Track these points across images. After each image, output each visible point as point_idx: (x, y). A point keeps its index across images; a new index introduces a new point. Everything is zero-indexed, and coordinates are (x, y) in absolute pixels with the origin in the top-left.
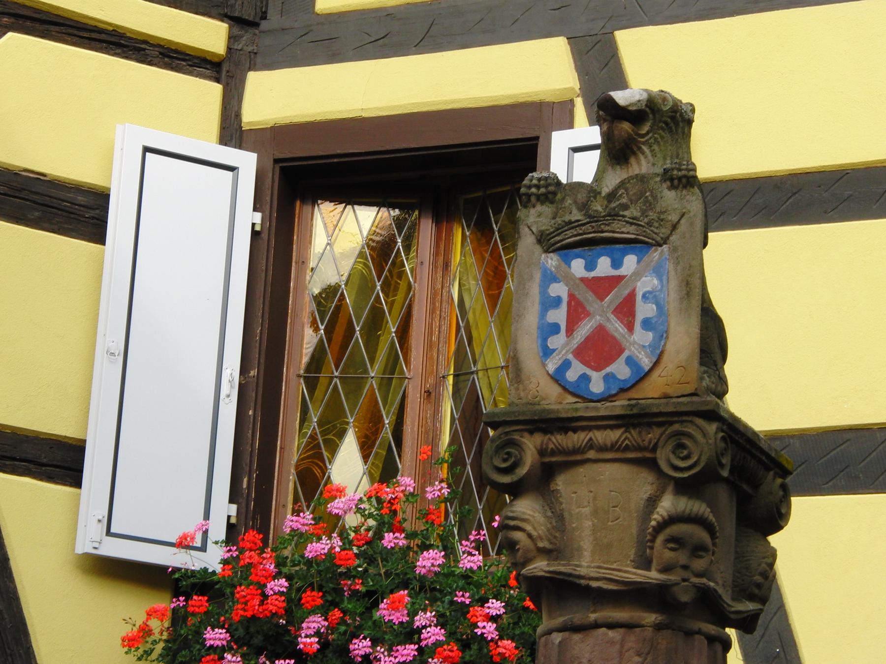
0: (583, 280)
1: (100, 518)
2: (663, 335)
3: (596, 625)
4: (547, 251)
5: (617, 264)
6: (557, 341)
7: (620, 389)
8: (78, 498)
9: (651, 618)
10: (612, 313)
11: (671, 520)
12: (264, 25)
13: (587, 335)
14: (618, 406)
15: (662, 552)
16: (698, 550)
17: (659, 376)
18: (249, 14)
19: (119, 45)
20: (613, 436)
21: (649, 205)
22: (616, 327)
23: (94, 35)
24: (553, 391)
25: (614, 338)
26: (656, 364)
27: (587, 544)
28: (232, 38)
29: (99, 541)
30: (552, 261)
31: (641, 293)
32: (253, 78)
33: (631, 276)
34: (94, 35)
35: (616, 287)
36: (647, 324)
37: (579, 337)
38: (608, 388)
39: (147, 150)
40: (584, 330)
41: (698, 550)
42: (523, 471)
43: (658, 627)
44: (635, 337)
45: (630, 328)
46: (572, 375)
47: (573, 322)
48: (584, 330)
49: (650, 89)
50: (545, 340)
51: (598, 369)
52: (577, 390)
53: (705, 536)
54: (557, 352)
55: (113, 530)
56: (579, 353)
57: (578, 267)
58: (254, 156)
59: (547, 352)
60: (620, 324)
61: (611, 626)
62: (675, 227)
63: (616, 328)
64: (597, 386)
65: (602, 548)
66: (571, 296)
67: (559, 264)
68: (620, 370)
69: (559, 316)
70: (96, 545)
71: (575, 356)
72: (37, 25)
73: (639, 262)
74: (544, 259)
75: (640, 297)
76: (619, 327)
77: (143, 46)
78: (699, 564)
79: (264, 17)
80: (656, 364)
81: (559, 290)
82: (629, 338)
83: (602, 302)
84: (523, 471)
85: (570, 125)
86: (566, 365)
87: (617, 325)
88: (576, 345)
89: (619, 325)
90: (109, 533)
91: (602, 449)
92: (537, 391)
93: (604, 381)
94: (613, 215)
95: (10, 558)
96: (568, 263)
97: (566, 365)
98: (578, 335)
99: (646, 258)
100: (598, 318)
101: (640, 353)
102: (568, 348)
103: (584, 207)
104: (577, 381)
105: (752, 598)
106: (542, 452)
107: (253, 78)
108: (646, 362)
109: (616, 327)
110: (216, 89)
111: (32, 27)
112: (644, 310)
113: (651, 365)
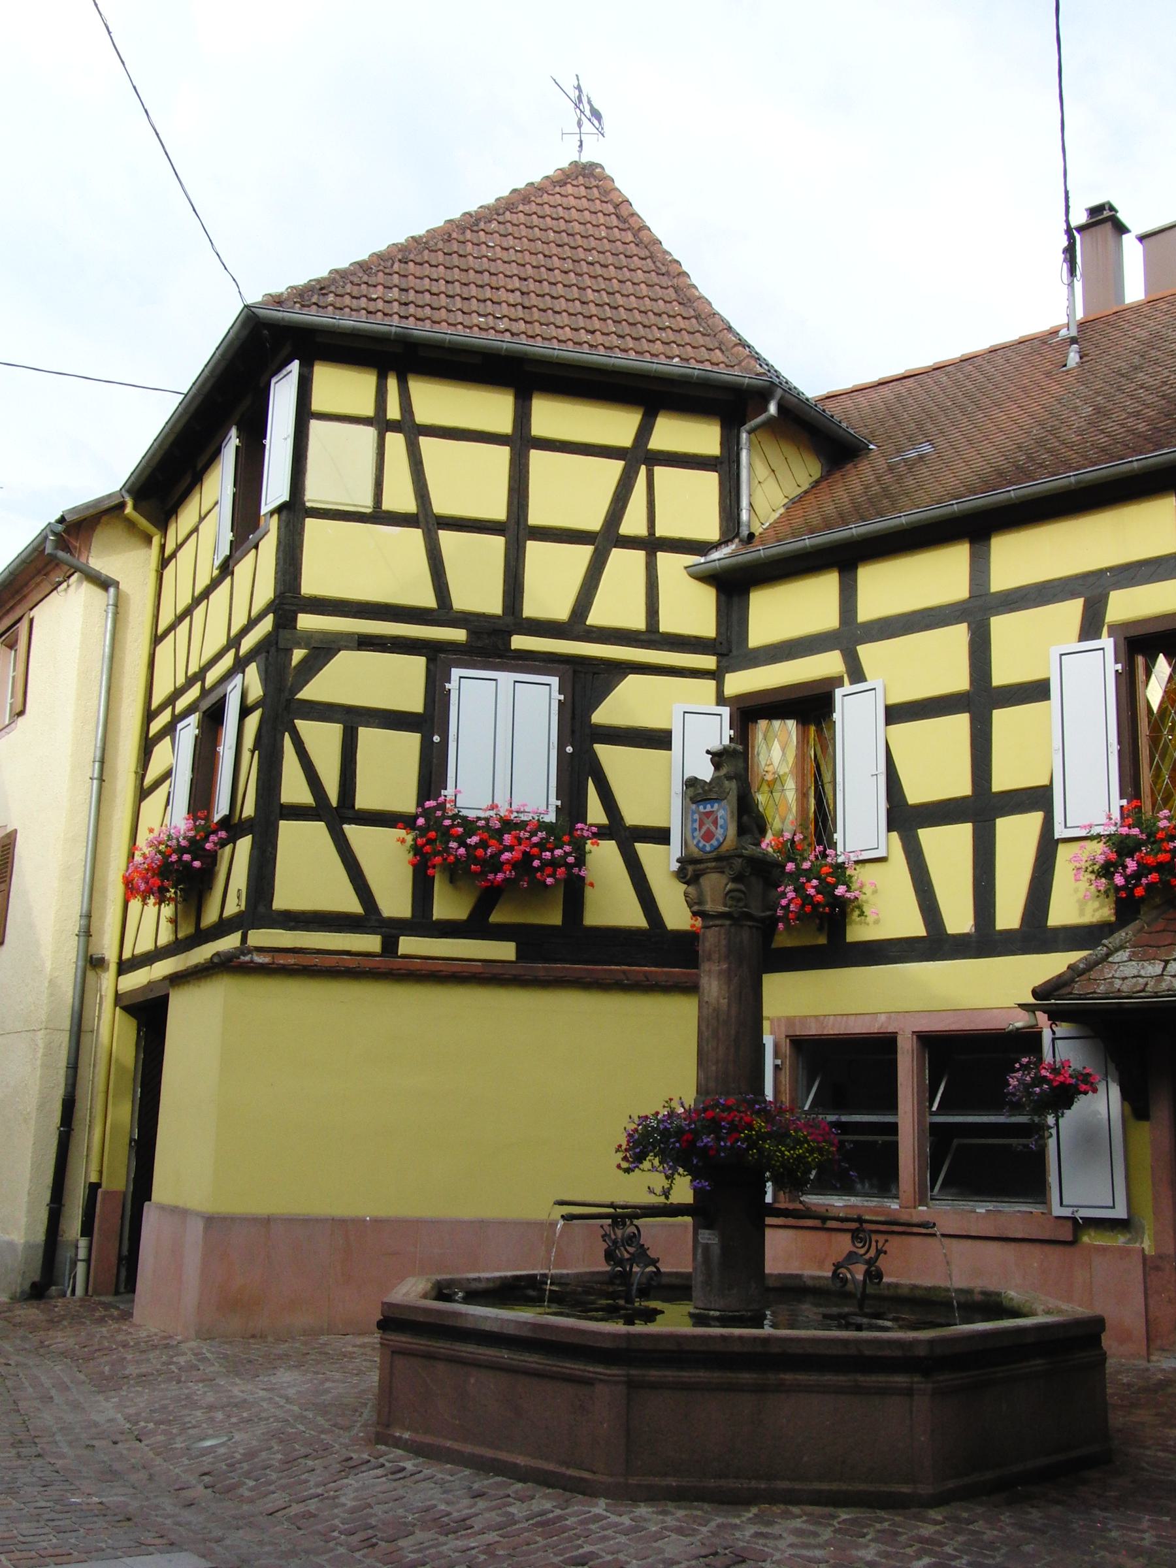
2: (726, 830)
3: (712, 926)
4: (693, 803)
5: (712, 807)
6: (696, 834)
9: (728, 922)
11: (731, 891)
12: (731, 654)
14: (713, 855)
15: (729, 902)
16: (739, 900)
18: (724, 651)
19: (673, 672)
20: (713, 864)
21: (721, 787)
22: (713, 828)
24: (697, 850)
26: (724, 840)
27: (709, 899)
28: (718, 662)
30: (694, 806)
32: (728, 676)
36: (721, 827)
39: (515, 682)
40: (704, 829)
41: (739, 900)
42: (688, 877)
43: (731, 925)
46: (701, 845)
48: (704, 829)
52: (702, 850)
53: (743, 896)
56: (703, 837)
57: (701, 807)
58: (728, 709)
59: (694, 838)
61: (716, 926)
62: (728, 793)
64: (708, 848)
65: (713, 901)
68: (714, 842)
69: (696, 825)
78: (741, 904)
79: (731, 651)
80: (724, 840)
81: (696, 816)
84: (688, 877)
85: (842, 685)
86: (699, 841)
91: (711, 869)
94: (710, 790)
96: (698, 806)
97: (699, 842)
103: (703, 788)
105: (771, 910)
106: (694, 871)
107: (728, 676)
108: (721, 840)
109: (713, 828)
110: (713, 683)
112: (721, 822)
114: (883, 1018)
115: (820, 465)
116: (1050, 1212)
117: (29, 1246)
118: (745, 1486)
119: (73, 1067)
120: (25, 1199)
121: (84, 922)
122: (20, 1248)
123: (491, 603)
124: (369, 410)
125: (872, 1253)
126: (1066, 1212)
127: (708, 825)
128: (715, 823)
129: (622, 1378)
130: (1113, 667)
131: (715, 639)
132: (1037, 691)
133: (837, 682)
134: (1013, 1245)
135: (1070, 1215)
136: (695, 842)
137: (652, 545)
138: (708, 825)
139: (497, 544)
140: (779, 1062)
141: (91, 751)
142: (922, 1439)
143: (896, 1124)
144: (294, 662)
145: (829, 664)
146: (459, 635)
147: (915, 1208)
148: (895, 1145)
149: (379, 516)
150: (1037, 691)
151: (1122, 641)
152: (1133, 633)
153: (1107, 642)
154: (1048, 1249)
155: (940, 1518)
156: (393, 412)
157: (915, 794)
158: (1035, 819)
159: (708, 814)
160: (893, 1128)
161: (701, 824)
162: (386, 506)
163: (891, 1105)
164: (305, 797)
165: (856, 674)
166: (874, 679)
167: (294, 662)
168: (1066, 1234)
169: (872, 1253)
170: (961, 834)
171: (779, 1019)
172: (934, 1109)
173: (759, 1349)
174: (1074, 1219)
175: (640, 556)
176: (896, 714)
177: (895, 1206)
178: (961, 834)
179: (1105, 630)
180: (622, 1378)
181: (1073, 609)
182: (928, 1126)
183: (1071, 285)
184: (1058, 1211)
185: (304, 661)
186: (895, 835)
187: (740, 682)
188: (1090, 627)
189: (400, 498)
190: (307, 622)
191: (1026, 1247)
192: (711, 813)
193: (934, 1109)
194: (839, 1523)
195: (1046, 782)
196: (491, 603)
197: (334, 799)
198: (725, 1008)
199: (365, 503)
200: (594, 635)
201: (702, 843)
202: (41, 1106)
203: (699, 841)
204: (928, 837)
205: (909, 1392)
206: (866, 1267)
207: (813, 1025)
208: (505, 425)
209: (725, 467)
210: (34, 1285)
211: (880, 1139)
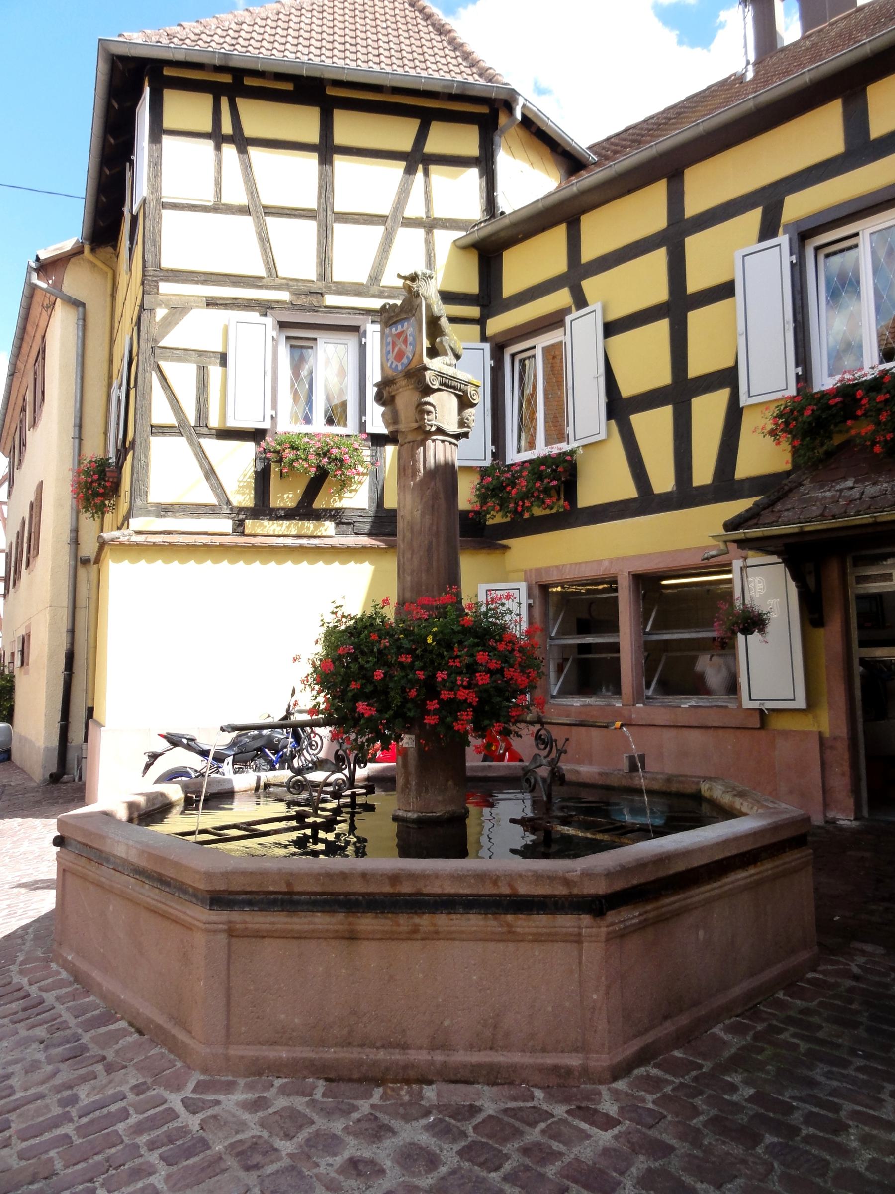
22: (403, 347)
28: (482, 312)
36: (411, 344)
56: (395, 358)
57: (394, 329)
64: (400, 368)
68: (405, 361)
69: (390, 348)
112: (410, 339)
114: (606, 563)
115: (559, 175)
116: (741, 705)
117: (47, 749)
118: (372, 1056)
119: (72, 632)
120: (43, 718)
121: (74, 535)
122: (42, 751)
123: (308, 271)
124: (208, 127)
125: (554, 754)
126: (755, 705)
127: (400, 345)
128: (405, 341)
129: (221, 926)
130: (787, 259)
131: (478, 295)
132: (725, 290)
133: (567, 311)
134: (711, 731)
135: (757, 707)
137: (430, 225)
138: (400, 345)
139: (310, 227)
140: (531, 601)
141: (71, 421)
142: (595, 997)
143: (618, 643)
144: (158, 319)
145: (562, 298)
146: (284, 296)
147: (634, 705)
148: (618, 660)
149: (218, 208)
150: (725, 290)
151: (795, 237)
153: (783, 239)
154: (738, 732)
156: (227, 128)
157: (627, 390)
158: (722, 396)
159: (399, 335)
160: (615, 648)
161: (394, 345)
162: (224, 200)
163: (613, 626)
164: (170, 419)
165: (580, 301)
166: (595, 305)
167: (158, 319)
168: (755, 722)
169: (554, 754)
170: (664, 415)
171: (531, 570)
172: (648, 630)
173: (387, 889)
174: (761, 711)
175: (421, 233)
176: (611, 329)
177: (619, 705)
178: (664, 415)
179: (781, 230)
180: (221, 926)
181: (754, 217)
184: (747, 704)
185: (165, 319)
186: (613, 422)
187: (498, 324)
188: (768, 230)
189: (236, 194)
190: (165, 288)
191: (721, 733)
192: (402, 332)
193: (648, 630)
194: (464, 1134)
195: (731, 363)
196: (308, 271)
197: (192, 420)
198: (418, 520)
199: (208, 198)
200: (386, 294)
201: (395, 363)
202: (51, 657)
204: (638, 420)
205: (577, 939)
206: (550, 768)
207: (555, 572)
208: (314, 137)
209: (483, 164)
210: (51, 775)
211: (609, 655)
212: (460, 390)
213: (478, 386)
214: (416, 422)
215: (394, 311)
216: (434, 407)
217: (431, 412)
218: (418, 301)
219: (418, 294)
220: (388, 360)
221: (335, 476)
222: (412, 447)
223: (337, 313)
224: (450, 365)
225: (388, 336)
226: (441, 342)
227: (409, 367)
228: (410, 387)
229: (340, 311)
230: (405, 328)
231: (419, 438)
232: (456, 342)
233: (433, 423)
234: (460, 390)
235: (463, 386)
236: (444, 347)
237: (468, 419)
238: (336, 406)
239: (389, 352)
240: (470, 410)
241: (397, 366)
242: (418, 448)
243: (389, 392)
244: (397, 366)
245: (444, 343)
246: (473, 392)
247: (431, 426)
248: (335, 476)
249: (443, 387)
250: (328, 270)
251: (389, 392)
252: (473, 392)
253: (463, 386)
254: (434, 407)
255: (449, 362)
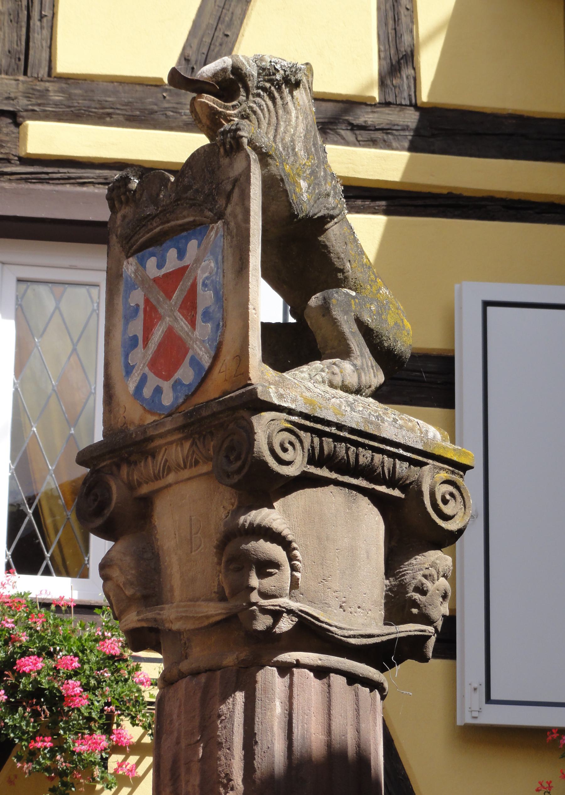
0: (156, 280)
1: (476, 685)
5: (181, 255)
7: (186, 396)
8: (455, 667)
10: (179, 311)
13: (159, 341)
17: (219, 372)
22: (182, 325)
23: (428, 202)
25: (180, 338)
26: (215, 359)
29: (478, 709)
31: (201, 281)
33: (193, 264)
34: (428, 202)
35: (181, 280)
36: (207, 315)
37: (153, 346)
38: (176, 398)
39: (486, 304)
44: (197, 333)
45: (193, 323)
47: (148, 330)
49: (246, 55)
50: (127, 356)
51: (167, 378)
54: (136, 367)
55: (493, 697)
56: (153, 365)
57: (152, 262)
60: (185, 321)
63: (182, 327)
64: (168, 399)
66: (147, 301)
67: (137, 268)
70: (475, 714)
71: (150, 369)
72: (367, 203)
73: (199, 245)
74: (126, 267)
75: (201, 285)
76: (184, 326)
77: (483, 203)
82: (191, 335)
83: (170, 300)
86: (143, 380)
87: (183, 323)
88: (151, 356)
89: (185, 324)
90: (488, 700)
92: (124, 417)
93: (173, 390)
95: (394, 739)
96: (142, 263)
98: (152, 344)
99: (204, 241)
100: (168, 319)
101: (201, 349)
102: (144, 362)
104: (151, 396)
108: (206, 361)
111: (362, 206)
113: (210, 361)
136: (132, 386)
152: (347, 183)
155: (333, 400)
182: (172, 88)
183: (169, 486)
192: (180, 272)
201: (153, 381)
203: (143, 380)
212: (392, 482)
213: (464, 468)
214: (222, 598)
215: (155, 200)
216: (286, 545)
217: (277, 565)
218: (238, 166)
219: (237, 139)
220: (129, 370)
221: (33, 755)
222: (206, 690)
223: (68, 180)
224: (358, 392)
225: (132, 287)
226: (325, 308)
227: (200, 399)
228: (205, 468)
229: (65, 171)
230: (188, 260)
231: (230, 660)
232: (383, 307)
233: (285, 602)
234: (392, 482)
235: (402, 468)
236: (334, 322)
237: (423, 591)
238: (50, 496)
239: (133, 342)
240: (434, 555)
241: (158, 391)
242: (224, 697)
243: (131, 487)
244: (158, 391)
245: (337, 313)
246: (443, 490)
247: (276, 615)
248: (33, 755)
249: (324, 472)
250: (38, 38)
251: (131, 487)
252: (443, 490)
253: (402, 468)
254: (286, 545)
255: (352, 380)
